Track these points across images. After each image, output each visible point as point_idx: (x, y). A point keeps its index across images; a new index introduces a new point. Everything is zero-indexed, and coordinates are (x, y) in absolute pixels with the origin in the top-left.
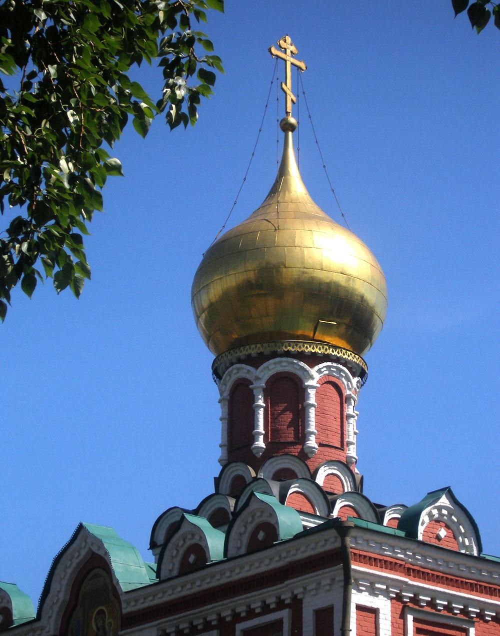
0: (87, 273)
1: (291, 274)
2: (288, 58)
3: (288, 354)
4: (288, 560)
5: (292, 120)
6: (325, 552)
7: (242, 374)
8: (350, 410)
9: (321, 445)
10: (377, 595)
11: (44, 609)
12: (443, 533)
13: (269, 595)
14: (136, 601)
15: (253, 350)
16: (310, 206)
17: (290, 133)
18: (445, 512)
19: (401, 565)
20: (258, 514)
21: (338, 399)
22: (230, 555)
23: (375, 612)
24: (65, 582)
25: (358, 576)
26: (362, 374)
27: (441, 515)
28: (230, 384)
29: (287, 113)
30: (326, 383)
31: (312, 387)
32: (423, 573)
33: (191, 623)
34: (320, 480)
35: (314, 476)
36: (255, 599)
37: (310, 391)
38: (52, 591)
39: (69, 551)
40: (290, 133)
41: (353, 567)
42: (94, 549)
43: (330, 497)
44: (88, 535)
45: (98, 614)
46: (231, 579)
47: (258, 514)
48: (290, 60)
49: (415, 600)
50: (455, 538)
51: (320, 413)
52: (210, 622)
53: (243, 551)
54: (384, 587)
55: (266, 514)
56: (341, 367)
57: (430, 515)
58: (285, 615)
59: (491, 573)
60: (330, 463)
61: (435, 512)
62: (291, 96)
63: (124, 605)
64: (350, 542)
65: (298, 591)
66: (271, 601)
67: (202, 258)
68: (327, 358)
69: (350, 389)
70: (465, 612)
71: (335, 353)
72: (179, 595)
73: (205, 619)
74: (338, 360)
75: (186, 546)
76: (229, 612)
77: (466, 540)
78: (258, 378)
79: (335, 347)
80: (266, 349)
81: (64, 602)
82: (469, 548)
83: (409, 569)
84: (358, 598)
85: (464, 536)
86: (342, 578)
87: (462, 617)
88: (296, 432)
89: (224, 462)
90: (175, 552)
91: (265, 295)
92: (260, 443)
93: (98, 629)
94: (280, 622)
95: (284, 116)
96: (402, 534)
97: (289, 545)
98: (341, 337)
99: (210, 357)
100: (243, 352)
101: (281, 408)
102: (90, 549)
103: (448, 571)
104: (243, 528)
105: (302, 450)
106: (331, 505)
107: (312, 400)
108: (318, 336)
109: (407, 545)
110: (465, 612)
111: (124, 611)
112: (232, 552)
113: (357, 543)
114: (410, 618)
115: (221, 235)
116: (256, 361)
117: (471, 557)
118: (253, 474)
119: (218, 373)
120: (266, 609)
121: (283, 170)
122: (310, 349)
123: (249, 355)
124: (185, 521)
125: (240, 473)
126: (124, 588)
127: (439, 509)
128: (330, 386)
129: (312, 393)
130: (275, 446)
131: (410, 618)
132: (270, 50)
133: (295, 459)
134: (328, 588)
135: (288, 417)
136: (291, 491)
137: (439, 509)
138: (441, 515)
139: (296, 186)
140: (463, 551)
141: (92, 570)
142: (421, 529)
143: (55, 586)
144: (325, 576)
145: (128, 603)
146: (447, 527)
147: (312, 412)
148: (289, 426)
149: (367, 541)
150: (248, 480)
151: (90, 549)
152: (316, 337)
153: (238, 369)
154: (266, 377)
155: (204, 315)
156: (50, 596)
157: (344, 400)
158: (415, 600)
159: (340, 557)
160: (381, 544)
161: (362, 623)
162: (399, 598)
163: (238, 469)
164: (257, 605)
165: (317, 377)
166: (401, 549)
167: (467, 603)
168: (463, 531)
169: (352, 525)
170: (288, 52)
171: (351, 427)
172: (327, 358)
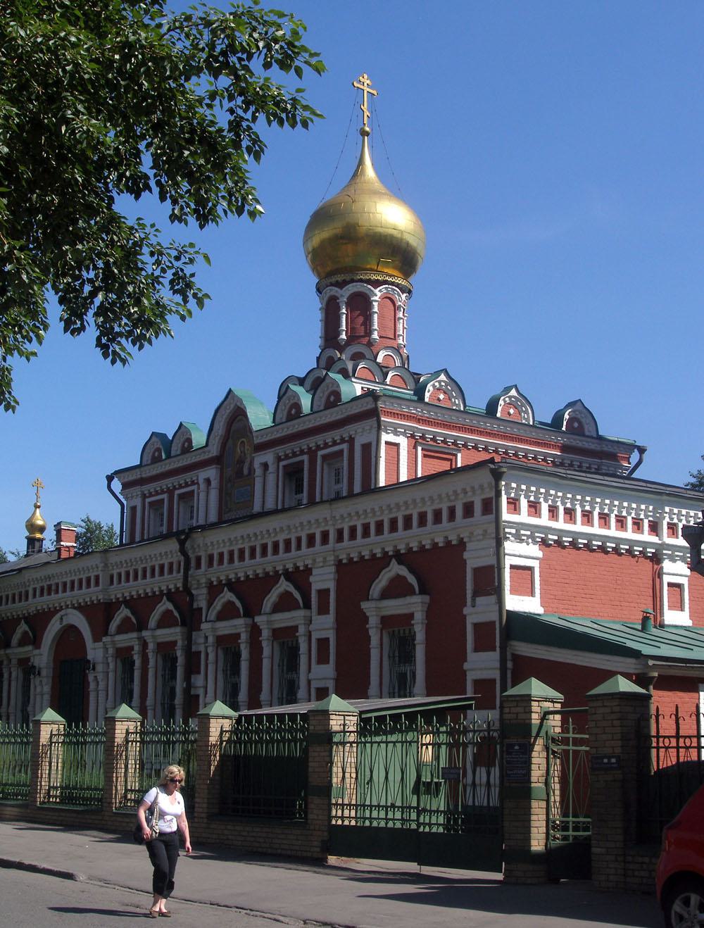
0: (18, 403)
1: (363, 230)
2: (365, 88)
3: (361, 281)
4: (347, 414)
5: (367, 129)
6: (367, 410)
7: (332, 293)
8: (400, 314)
10: (399, 436)
11: (210, 441)
12: (442, 397)
13: (336, 434)
14: (262, 436)
15: (340, 278)
16: (378, 185)
17: (366, 137)
18: (443, 384)
19: (414, 417)
20: (330, 385)
21: (393, 308)
22: (315, 409)
23: (397, 445)
24: (222, 424)
25: (385, 424)
26: (410, 292)
27: (441, 385)
28: (326, 299)
29: (364, 124)
30: (386, 298)
31: (376, 301)
32: (428, 421)
33: (293, 450)
34: (380, 359)
35: (376, 357)
36: (328, 437)
37: (374, 303)
38: (214, 428)
39: (224, 405)
40: (366, 137)
41: (382, 419)
42: (238, 404)
43: (385, 370)
44: (235, 396)
45: (241, 443)
46: (315, 425)
47: (330, 385)
48: (366, 89)
49: (423, 437)
50: (450, 399)
52: (336, 441)
53: (322, 408)
54: (403, 430)
55: (335, 386)
56: (394, 287)
57: (434, 386)
58: (345, 446)
59: (471, 420)
60: (386, 348)
61: (437, 384)
62: (367, 113)
64: (380, 404)
66: (337, 438)
67: (309, 219)
68: (385, 282)
69: (400, 301)
70: (455, 444)
71: (391, 279)
72: (286, 434)
73: (300, 448)
74: (393, 284)
75: (290, 404)
76: (314, 444)
77: (457, 400)
78: (342, 296)
79: (391, 276)
80: (348, 278)
81: (221, 436)
82: (458, 405)
83: (419, 419)
84: (385, 437)
85: (455, 398)
86: (376, 426)
87: (453, 447)
88: (366, 328)
89: (322, 348)
90: (284, 408)
91: (346, 244)
92: (344, 336)
93: (241, 452)
94: (342, 451)
95: (362, 126)
96: (416, 398)
97: (346, 405)
98: (395, 268)
99: (315, 280)
100: (333, 280)
101: (357, 314)
102: (236, 405)
103: (444, 420)
104: (323, 392)
105: (369, 340)
106: (386, 375)
107: (376, 309)
108: (380, 269)
109: (419, 405)
110: (455, 444)
111: (255, 442)
112: (315, 409)
113: (386, 405)
114: (419, 448)
115: (321, 204)
116: (341, 285)
117: (460, 411)
118: (339, 356)
119: (319, 290)
120: (335, 443)
121: (361, 162)
122: (374, 278)
123: (337, 281)
124: (289, 390)
125: (332, 355)
126: (255, 428)
127: (440, 382)
128: (388, 300)
129: (375, 304)
130: (352, 339)
131: (419, 448)
132: (353, 84)
133: (365, 346)
134: (368, 431)
135: (361, 319)
136: (359, 367)
137: (440, 382)
138: (441, 385)
139: (370, 172)
140: (454, 408)
141: (238, 416)
142: (427, 395)
143: (216, 426)
145: (257, 437)
146: (445, 393)
147: (376, 316)
148: (361, 325)
149: (392, 403)
150: (336, 359)
151: (236, 405)
153: (331, 290)
154: (348, 295)
155: (310, 256)
156: (213, 432)
157: (396, 308)
158: (423, 437)
159: (374, 413)
160: (401, 405)
161: (389, 452)
162: (413, 436)
163: (330, 352)
164: (329, 441)
165: (379, 294)
166: (414, 407)
167: (456, 439)
168: (455, 395)
169: (382, 394)
170: (365, 84)
171: (400, 326)
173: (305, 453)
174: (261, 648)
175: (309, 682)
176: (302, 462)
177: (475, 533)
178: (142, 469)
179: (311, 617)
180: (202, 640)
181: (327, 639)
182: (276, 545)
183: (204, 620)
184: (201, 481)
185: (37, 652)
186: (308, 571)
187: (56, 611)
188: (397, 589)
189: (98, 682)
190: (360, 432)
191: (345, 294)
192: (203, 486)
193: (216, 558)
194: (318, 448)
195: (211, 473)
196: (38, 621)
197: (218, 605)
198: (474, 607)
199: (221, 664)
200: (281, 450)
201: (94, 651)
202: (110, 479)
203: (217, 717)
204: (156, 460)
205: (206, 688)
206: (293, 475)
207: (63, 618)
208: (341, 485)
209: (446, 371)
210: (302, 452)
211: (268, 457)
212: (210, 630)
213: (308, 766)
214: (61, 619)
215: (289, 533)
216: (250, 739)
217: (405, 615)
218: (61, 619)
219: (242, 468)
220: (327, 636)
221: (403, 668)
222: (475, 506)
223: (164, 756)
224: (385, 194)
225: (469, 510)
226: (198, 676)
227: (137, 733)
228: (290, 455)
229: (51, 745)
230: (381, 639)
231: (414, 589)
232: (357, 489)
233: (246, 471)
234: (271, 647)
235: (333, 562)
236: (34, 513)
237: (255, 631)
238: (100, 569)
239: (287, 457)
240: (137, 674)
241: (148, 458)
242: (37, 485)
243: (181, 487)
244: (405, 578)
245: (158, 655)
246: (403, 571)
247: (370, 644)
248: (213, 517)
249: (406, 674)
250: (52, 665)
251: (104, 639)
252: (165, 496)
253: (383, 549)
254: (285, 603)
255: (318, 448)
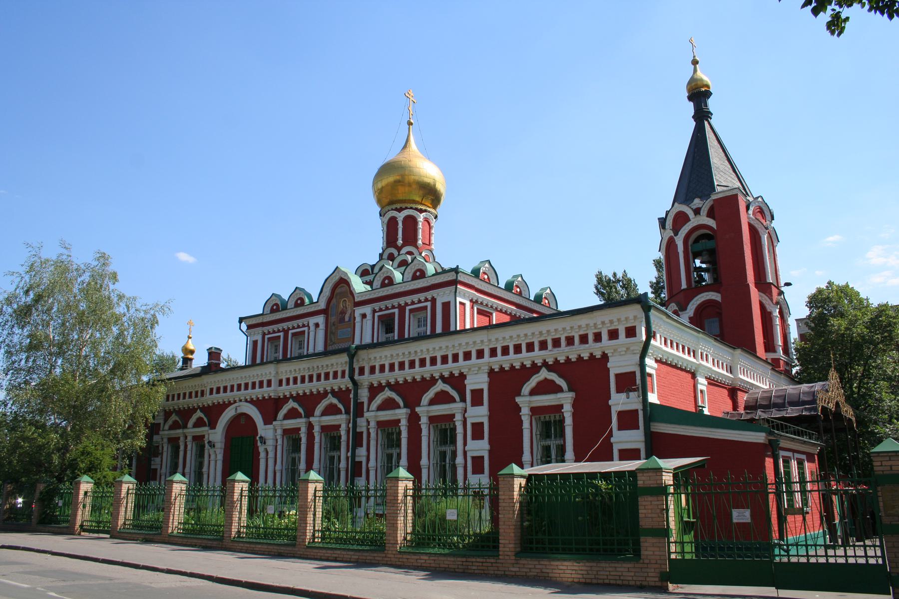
5: (412, 121)
7: (393, 215)
9: (423, 243)
13: (422, 296)
15: (398, 206)
16: (419, 154)
36: (415, 298)
42: (343, 276)
51: (423, 231)
63: (356, 298)
65: (435, 296)
80: (403, 206)
84: (459, 299)
86: (454, 291)
98: (431, 204)
99: (378, 209)
100: (394, 207)
116: (400, 210)
120: (420, 302)
121: (408, 140)
123: (396, 208)
129: (420, 223)
137: (486, 268)
143: (324, 290)
144: (450, 289)
147: (420, 231)
152: (423, 202)
172: (425, 211)
173: (281, 332)
174: (421, 430)
175: (465, 453)
176: (394, 313)
177: (619, 350)
178: (264, 316)
179: (466, 408)
180: (365, 424)
181: (482, 424)
182: (232, 387)
183: (161, 429)
184: (311, 325)
185: (213, 431)
186: (462, 376)
187: (230, 404)
188: (331, 410)
189: (216, 455)
190: (442, 296)
191: (400, 216)
192: (312, 328)
193: (182, 395)
194: (407, 304)
195: (320, 319)
196: (213, 413)
197: (170, 422)
198: (628, 398)
199: (169, 453)
200: (376, 306)
201: (263, 430)
202: (241, 320)
203: (239, 481)
204: (273, 311)
205: (161, 465)
206: (387, 323)
207: (238, 408)
208: (278, 354)
209: (490, 262)
210: (393, 307)
211: (367, 310)
212: (372, 416)
213: (638, 513)
214: (236, 409)
215: (313, 371)
216: (150, 493)
217: (176, 438)
218: (236, 409)
219: (344, 317)
220: (482, 421)
221: (293, 455)
222: (562, 341)
223: (152, 503)
224: (422, 158)
225: (467, 356)
226: (361, 448)
227: (133, 489)
228: (416, 302)
229: (127, 497)
230: (377, 434)
231: (341, 410)
232: (439, 330)
233: (347, 319)
234: (428, 428)
235: (487, 371)
236: (187, 342)
237: (310, 427)
238: (272, 375)
239: (381, 310)
240: (181, 454)
241: (268, 310)
242: (190, 323)
243: (294, 328)
244: (297, 409)
245: (285, 437)
246: (296, 405)
247: (522, 426)
248: (320, 348)
249: (334, 457)
250: (224, 440)
251: (274, 423)
252: (281, 334)
253: (291, 393)
254: (442, 398)
255: (289, 329)
